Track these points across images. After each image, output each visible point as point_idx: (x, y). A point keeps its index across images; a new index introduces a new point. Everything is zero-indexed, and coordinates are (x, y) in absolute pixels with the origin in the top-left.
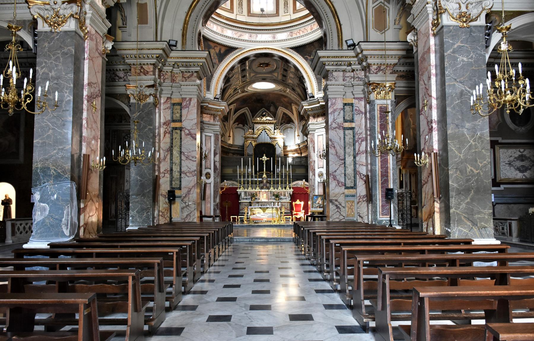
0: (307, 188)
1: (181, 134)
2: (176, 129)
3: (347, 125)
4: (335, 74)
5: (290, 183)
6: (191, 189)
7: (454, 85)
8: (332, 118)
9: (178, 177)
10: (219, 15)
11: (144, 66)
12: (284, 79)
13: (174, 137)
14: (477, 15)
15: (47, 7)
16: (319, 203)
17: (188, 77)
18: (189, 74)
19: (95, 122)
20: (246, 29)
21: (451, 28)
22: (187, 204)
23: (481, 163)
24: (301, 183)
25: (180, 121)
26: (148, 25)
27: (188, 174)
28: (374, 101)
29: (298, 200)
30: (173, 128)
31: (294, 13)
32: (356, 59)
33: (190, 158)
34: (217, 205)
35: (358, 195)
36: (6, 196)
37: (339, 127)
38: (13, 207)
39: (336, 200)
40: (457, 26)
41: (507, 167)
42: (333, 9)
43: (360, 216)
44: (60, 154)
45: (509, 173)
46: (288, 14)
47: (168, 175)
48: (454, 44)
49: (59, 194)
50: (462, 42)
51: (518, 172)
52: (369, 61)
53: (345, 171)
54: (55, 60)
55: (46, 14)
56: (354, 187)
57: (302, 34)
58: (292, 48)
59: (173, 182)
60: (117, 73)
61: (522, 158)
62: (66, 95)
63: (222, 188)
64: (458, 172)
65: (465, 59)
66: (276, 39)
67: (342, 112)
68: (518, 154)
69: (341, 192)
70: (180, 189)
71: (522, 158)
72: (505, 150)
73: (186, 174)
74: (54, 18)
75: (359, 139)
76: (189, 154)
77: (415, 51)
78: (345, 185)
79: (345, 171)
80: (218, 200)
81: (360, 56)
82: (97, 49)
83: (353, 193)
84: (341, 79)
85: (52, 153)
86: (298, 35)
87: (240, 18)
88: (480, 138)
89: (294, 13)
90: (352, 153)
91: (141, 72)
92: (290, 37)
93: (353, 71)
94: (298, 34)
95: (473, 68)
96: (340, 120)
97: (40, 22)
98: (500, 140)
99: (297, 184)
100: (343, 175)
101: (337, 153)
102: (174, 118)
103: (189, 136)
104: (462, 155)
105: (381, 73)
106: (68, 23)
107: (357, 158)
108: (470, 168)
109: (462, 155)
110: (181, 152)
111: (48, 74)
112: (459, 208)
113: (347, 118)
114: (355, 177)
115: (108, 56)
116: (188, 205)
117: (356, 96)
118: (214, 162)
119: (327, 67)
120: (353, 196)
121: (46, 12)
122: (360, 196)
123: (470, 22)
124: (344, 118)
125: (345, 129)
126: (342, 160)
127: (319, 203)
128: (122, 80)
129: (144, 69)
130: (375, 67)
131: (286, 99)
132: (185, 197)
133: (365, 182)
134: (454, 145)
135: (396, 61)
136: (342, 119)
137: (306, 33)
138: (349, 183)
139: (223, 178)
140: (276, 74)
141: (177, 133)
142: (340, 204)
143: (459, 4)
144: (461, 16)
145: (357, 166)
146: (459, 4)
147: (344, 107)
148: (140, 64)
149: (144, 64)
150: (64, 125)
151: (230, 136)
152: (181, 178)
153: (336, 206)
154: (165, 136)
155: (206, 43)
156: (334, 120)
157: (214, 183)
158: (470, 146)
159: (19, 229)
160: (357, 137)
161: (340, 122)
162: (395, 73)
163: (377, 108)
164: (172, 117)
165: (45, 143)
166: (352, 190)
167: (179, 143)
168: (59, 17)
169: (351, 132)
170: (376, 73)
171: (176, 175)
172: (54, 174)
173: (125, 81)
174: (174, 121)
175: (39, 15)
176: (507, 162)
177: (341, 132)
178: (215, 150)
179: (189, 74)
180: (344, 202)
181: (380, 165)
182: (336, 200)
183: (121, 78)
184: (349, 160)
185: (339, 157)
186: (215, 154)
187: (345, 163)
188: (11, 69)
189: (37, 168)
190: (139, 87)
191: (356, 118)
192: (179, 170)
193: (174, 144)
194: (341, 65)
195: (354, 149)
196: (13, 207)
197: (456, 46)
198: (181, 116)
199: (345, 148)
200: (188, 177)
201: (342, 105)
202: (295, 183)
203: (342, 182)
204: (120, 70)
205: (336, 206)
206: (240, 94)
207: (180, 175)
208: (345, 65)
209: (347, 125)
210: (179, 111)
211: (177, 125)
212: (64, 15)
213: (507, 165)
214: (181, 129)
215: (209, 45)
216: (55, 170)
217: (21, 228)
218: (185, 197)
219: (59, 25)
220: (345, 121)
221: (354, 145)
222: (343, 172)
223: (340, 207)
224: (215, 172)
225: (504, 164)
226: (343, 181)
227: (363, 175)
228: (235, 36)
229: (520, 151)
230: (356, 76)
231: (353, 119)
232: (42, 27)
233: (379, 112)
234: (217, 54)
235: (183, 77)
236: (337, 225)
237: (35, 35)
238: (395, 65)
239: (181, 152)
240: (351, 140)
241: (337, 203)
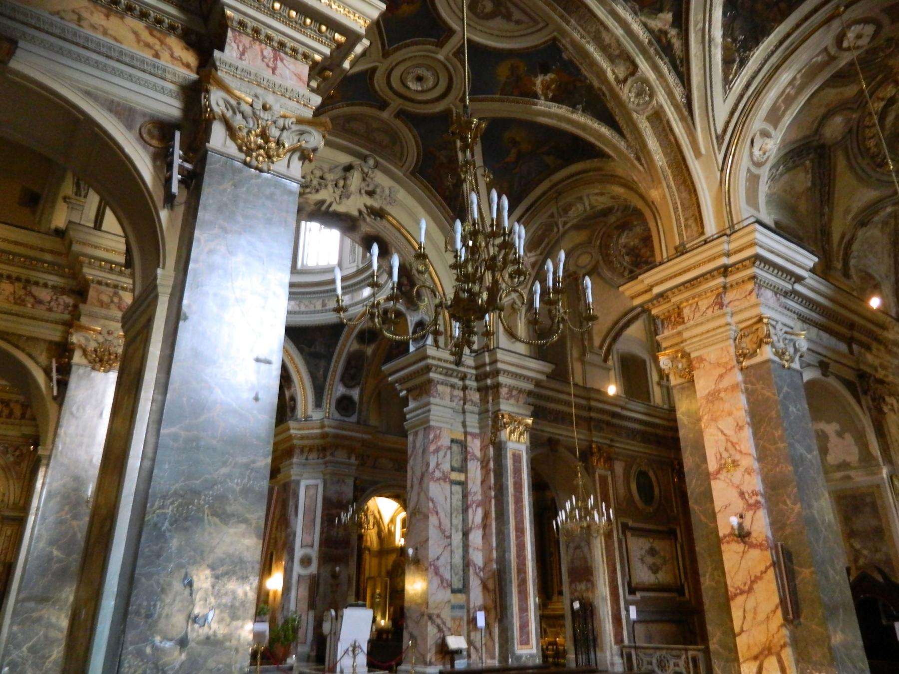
3: (455, 476)
4: (440, 388)
8: (435, 460)
11: (121, 292)
28: (505, 443)
32: (474, 372)
37: (445, 478)
45: (643, 575)
52: (502, 379)
56: (464, 589)
67: (449, 452)
69: (446, 600)
75: (474, 502)
81: (488, 368)
84: (448, 398)
90: (460, 527)
91: (112, 301)
92: (297, 309)
93: (465, 388)
96: (446, 467)
98: (630, 524)
101: (440, 523)
105: (512, 401)
119: (432, 375)
138: (457, 584)
142: (444, 623)
145: (471, 551)
153: (438, 626)
156: (438, 465)
161: (446, 470)
170: (508, 399)
183: (40, 302)
184: (457, 538)
185: (443, 531)
190: (105, 332)
194: (451, 376)
195: (465, 521)
201: (449, 441)
203: (447, 580)
205: (438, 626)
208: (456, 377)
209: (455, 476)
220: (453, 469)
230: (468, 397)
236: (332, 658)
240: (460, 504)
241: (438, 621)
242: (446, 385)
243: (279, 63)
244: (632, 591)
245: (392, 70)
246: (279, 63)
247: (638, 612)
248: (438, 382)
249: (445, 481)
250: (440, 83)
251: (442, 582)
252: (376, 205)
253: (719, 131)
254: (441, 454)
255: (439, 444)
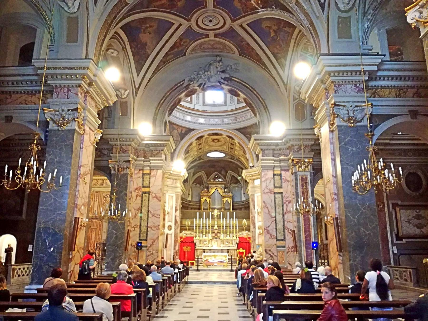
0: (249, 238)
1: (149, 197)
2: (145, 193)
5: (236, 233)
6: (155, 240)
7: (347, 168)
8: (265, 184)
9: (146, 230)
10: (181, 106)
11: (123, 147)
12: (231, 150)
13: (143, 199)
14: (361, 119)
15: (57, 113)
16: (260, 252)
17: (156, 154)
18: (156, 152)
19: (85, 193)
20: (201, 115)
21: (343, 127)
22: (151, 253)
23: (371, 226)
24: (245, 234)
25: (149, 187)
26: (127, 117)
27: (153, 228)
29: (241, 249)
30: (143, 192)
31: (238, 103)
33: (156, 215)
34: (176, 252)
35: (287, 246)
36: (9, 245)
38: (14, 254)
39: (270, 250)
40: (347, 126)
41: (407, 224)
42: (264, 105)
43: (289, 264)
44: (58, 217)
45: (408, 229)
46: (233, 104)
47: (138, 230)
48: (315, 160)
49: (54, 248)
50: (351, 137)
51: (416, 228)
53: (276, 226)
54: (60, 150)
55: (56, 118)
56: (284, 240)
57: (244, 119)
58: (237, 130)
59: (141, 235)
60: (102, 151)
61: (418, 217)
62: (66, 174)
63: (181, 238)
64: (354, 233)
65: (354, 149)
66: (224, 123)
67: (273, 180)
68: (415, 214)
70: (146, 240)
71: (418, 217)
72: (405, 211)
73: (151, 228)
74: (61, 120)
75: (287, 201)
76: (155, 212)
77: (320, 140)
78: (277, 238)
79: (276, 226)
80: (177, 248)
82: (90, 140)
83: (284, 245)
85: (52, 217)
86: (241, 119)
87: (197, 107)
88: (369, 207)
89: (238, 103)
90: (281, 212)
94: (241, 119)
95: (361, 155)
97: (51, 123)
99: (242, 234)
100: (275, 230)
101: (269, 212)
102: (144, 185)
103: (155, 199)
104: (355, 220)
106: (71, 124)
107: (285, 216)
108: (363, 229)
109: (355, 220)
110: (148, 211)
111: (54, 160)
112: (356, 260)
113: (276, 185)
114: (284, 231)
115: (97, 144)
116: (152, 254)
117: (283, 168)
118: (175, 217)
120: (284, 247)
121: (56, 116)
122: (289, 247)
123: (356, 123)
124: (274, 185)
125: (275, 193)
126: (273, 217)
127: (260, 252)
128: (106, 156)
129: (123, 149)
130: (297, 147)
131: (234, 165)
132: (150, 247)
133: (292, 235)
134: (349, 212)
135: (313, 143)
136: (273, 186)
137: (247, 118)
139: (183, 228)
140: (225, 147)
141: (146, 196)
142: (273, 254)
143: (348, 111)
144: (349, 119)
145: (286, 223)
146: (348, 111)
147: (274, 176)
148: (120, 145)
149: (123, 145)
150: (62, 196)
151: (189, 194)
152: (147, 231)
153: (270, 255)
154: (136, 198)
155: (171, 126)
157: (175, 234)
158: (362, 212)
159: (17, 273)
160: (284, 200)
161: (271, 188)
162: (312, 152)
163: (299, 178)
164: (143, 184)
165: (48, 209)
166: (282, 242)
167: (147, 204)
168: (65, 120)
169: (280, 195)
170: (298, 152)
171: (144, 229)
172: (52, 232)
173: (108, 157)
174: (144, 187)
175: (51, 118)
176: (407, 220)
177: (273, 195)
178: (176, 207)
179: (156, 152)
180: (276, 252)
181: (303, 222)
182: (270, 250)
183: (105, 155)
184: (279, 218)
186: (176, 210)
187: (276, 220)
188: (32, 163)
189: (40, 228)
191: (284, 184)
192: (146, 225)
193: (143, 205)
195: (283, 209)
196: (14, 254)
197: (347, 140)
198: (150, 183)
199: (275, 208)
200: (153, 230)
202: (240, 233)
203: (274, 236)
204: (105, 149)
205: (270, 255)
206: (198, 161)
207: (147, 229)
209: (277, 190)
210: (148, 180)
211: (147, 190)
212: (69, 119)
213: (407, 223)
214: (149, 193)
215: (173, 127)
216: (53, 229)
217: (19, 272)
218: (150, 247)
219: (64, 126)
220: (275, 187)
221: (283, 206)
222: (275, 227)
223: (273, 255)
224: (175, 225)
225: (404, 222)
226: (275, 235)
227: (291, 230)
228: (193, 121)
229: (416, 212)
231: (281, 186)
232: (52, 126)
233: (301, 181)
234: (179, 134)
235: (152, 154)
237: (47, 132)
238: (312, 145)
239: (148, 211)
240: (281, 202)
241: (270, 253)
242: (270, 150)
243: (69, 92)
244: (399, 238)
245: (198, 19)
246: (69, 92)
247: (398, 250)
248: (265, 150)
249: (271, 193)
250: (198, 28)
251: (271, 237)
252: (228, 76)
253: (137, 87)
254: (268, 182)
255: (267, 177)
